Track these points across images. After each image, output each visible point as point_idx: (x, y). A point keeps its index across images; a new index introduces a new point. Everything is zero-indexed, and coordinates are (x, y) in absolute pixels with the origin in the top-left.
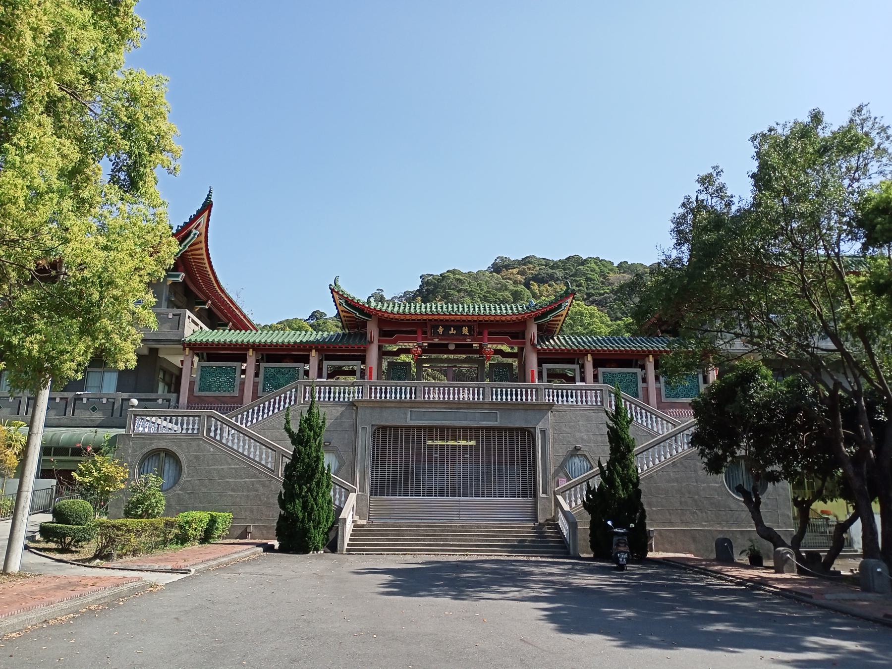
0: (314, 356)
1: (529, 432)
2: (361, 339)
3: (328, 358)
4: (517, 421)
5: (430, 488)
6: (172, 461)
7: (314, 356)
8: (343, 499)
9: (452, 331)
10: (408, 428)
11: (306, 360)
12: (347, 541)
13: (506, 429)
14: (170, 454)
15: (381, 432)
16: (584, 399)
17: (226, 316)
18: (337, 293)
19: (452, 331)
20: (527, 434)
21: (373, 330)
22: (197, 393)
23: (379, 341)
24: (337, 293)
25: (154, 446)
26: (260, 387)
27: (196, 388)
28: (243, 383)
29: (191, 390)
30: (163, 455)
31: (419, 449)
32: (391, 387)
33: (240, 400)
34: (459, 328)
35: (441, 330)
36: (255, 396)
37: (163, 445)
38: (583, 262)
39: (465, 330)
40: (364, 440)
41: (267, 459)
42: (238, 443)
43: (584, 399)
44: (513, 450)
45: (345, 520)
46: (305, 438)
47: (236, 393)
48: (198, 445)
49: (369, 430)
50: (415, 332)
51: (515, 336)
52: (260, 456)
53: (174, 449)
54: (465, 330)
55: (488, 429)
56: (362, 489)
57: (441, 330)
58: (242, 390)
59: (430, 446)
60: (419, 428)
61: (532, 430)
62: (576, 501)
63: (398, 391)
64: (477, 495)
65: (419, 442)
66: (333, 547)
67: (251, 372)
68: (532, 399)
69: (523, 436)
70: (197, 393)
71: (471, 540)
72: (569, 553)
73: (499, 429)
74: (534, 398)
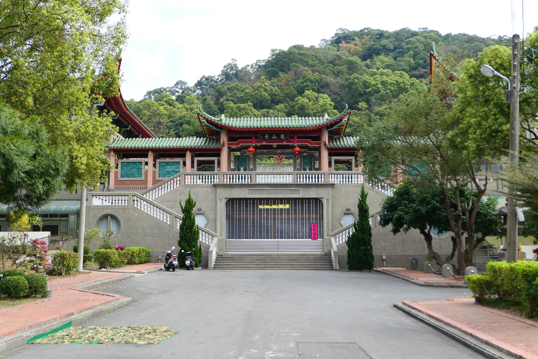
0: (188, 155)
1: (320, 201)
2: (217, 143)
3: (197, 156)
4: (312, 194)
5: (289, 234)
6: (114, 221)
7: (188, 155)
8: (210, 241)
9: (274, 137)
10: (247, 199)
11: (184, 156)
12: (213, 263)
13: (306, 199)
14: (113, 217)
15: (231, 202)
16: (350, 180)
17: (127, 121)
18: (201, 116)
19: (274, 137)
20: (318, 201)
21: (224, 138)
22: (119, 178)
23: (229, 144)
24: (201, 116)
25: (105, 213)
26: (157, 175)
27: (119, 176)
28: (146, 172)
29: (116, 177)
30: (109, 217)
31: (254, 211)
32: (236, 175)
33: (146, 182)
34: (278, 135)
35: (267, 136)
36: (155, 182)
37: (109, 212)
38: (414, 34)
39: (282, 136)
40: (221, 208)
41: (166, 219)
42: (160, 215)
43: (350, 180)
44: (308, 210)
45: (212, 252)
46: (188, 209)
47: (143, 178)
48: (129, 212)
49: (224, 201)
50: (251, 138)
51: (314, 139)
52: (163, 218)
53: (116, 214)
54: (282, 136)
55: (295, 199)
56: (221, 235)
57: (267, 136)
58: (146, 176)
59: (261, 210)
60: (254, 199)
61: (321, 199)
62: (342, 240)
63: (242, 177)
64: (296, 238)
65: (254, 207)
66: (206, 266)
67: (151, 163)
68: (322, 181)
69: (316, 203)
70: (119, 178)
71: (281, 262)
72: (333, 268)
73: (302, 199)
74: (323, 179)
